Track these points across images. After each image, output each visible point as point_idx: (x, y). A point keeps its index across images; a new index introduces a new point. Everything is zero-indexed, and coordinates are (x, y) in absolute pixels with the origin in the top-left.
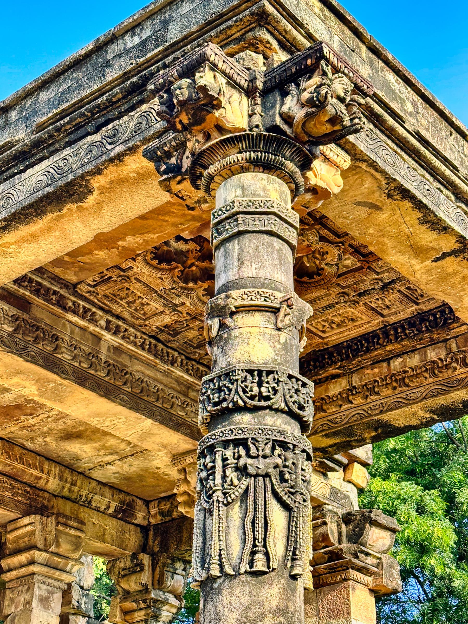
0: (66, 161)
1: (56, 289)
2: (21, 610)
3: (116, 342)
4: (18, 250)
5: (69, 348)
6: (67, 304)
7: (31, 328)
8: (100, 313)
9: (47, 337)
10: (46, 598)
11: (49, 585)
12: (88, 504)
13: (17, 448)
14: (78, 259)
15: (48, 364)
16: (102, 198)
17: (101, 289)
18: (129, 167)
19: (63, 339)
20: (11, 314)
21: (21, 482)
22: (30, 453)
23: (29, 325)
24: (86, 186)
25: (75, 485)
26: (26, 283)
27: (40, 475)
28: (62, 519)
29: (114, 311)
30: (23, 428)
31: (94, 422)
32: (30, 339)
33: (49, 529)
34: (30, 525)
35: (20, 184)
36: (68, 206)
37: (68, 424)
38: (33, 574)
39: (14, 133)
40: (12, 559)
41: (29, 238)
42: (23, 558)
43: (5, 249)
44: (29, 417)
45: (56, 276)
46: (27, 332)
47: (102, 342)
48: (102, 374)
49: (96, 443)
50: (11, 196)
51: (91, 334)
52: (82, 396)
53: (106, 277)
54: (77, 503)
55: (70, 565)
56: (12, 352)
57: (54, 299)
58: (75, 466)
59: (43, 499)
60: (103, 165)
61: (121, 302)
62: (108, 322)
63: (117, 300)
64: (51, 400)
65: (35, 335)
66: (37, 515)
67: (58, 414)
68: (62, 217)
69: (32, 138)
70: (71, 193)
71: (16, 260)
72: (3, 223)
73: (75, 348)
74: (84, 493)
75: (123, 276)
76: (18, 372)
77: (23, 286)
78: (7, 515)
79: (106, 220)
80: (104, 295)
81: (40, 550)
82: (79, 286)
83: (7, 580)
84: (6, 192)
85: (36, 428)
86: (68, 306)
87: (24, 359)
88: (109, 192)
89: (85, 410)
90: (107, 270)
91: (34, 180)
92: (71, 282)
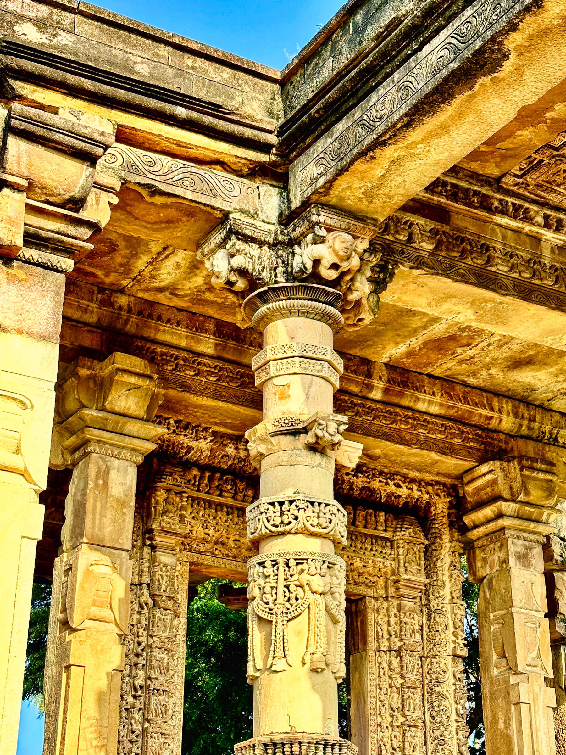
0: (469, 24)
1: (476, 188)
2: (497, 571)
3: (560, 240)
4: (427, 149)
5: (504, 258)
6: (493, 204)
7: (454, 242)
8: (535, 208)
9: (475, 249)
10: (524, 554)
11: (525, 539)
12: (554, 441)
13: (458, 387)
14: (498, 146)
15: (482, 281)
16: (521, 61)
17: (532, 179)
18: (551, 12)
19: (494, 248)
20: (428, 229)
21: (470, 425)
22: (474, 390)
23: (452, 237)
24: (500, 50)
25: (534, 421)
26: (440, 188)
27: (490, 414)
28: (526, 462)
29: (551, 202)
30: (462, 361)
31: (548, 342)
32: (455, 254)
33: (512, 475)
34: (489, 474)
35: (418, 67)
36: (481, 81)
37: (514, 350)
38: (503, 529)
39: (399, 6)
40: (475, 514)
41: (439, 131)
42: (488, 512)
43: (412, 151)
44: (465, 349)
45: (473, 172)
46: (451, 247)
47: (543, 244)
48: (549, 282)
49: (552, 367)
50: (410, 85)
51: (527, 235)
52: (529, 313)
53: (535, 162)
54: (540, 442)
55: (545, 514)
56: (437, 274)
57: (476, 201)
58: (530, 398)
59: (499, 441)
60: (517, 17)
61: (558, 189)
62: (546, 217)
63: (553, 187)
64: (492, 324)
65: (460, 249)
66: (496, 461)
67: (501, 340)
68: (474, 96)
69: (422, 6)
70: (482, 63)
71: (427, 162)
72: (405, 119)
73: (511, 257)
74: (547, 428)
75: (557, 156)
76: (449, 296)
77: (437, 193)
78: (460, 465)
79: (530, 87)
80: (535, 185)
81: (506, 500)
82: (503, 180)
83: (474, 538)
84: (403, 81)
85: (476, 359)
86: (494, 206)
87: (453, 279)
88: (529, 52)
89: (534, 330)
90: (536, 152)
91: (434, 58)
92: (493, 176)
